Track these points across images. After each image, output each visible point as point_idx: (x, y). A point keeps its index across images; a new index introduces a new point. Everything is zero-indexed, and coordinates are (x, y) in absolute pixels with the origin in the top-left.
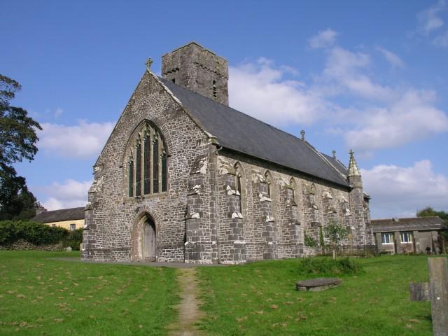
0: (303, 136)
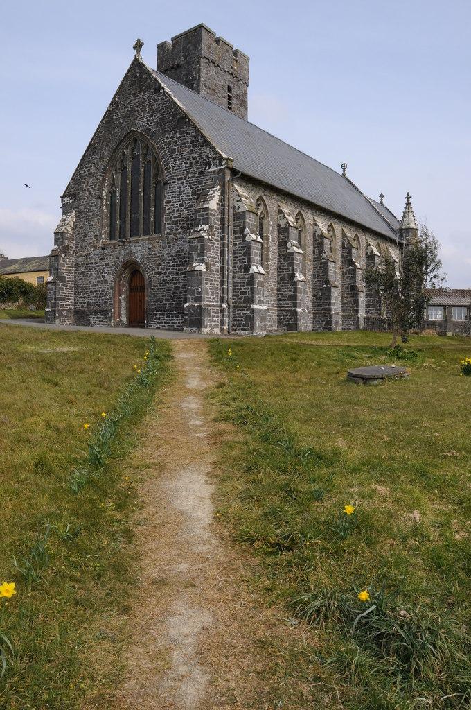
0: (344, 171)
